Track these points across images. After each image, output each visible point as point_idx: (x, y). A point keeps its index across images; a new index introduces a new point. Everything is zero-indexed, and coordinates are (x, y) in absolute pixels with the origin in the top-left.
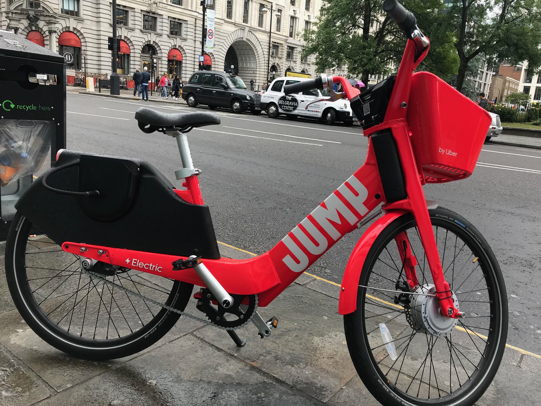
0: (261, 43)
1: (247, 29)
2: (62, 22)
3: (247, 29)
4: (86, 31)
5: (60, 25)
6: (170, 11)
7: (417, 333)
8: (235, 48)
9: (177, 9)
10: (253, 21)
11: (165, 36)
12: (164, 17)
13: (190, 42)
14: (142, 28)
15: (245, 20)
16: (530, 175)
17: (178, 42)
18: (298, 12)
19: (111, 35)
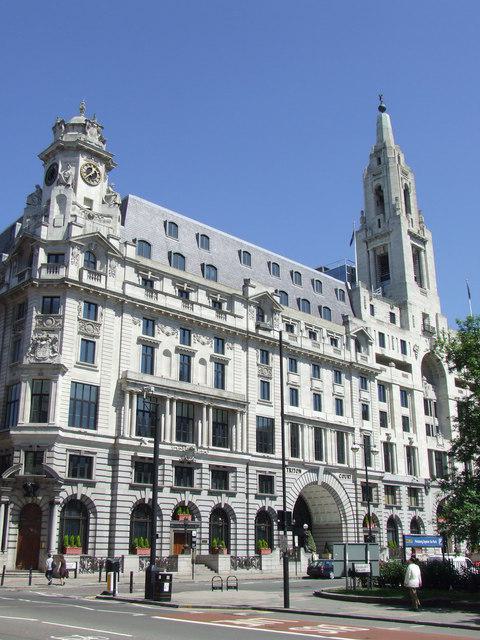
0: (345, 486)
1: (322, 469)
2: (68, 488)
3: (322, 469)
4: (99, 497)
5: (66, 492)
6: (213, 458)
7: (52, 140)
8: (306, 497)
9: (223, 452)
10: (331, 458)
11: (204, 493)
12: (204, 466)
13: (241, 497)
14: (132, 481)
15: (319, 455)
16: (286, 257)
17: (224, 500)
18: (392, 436)
19: (282, 509)
